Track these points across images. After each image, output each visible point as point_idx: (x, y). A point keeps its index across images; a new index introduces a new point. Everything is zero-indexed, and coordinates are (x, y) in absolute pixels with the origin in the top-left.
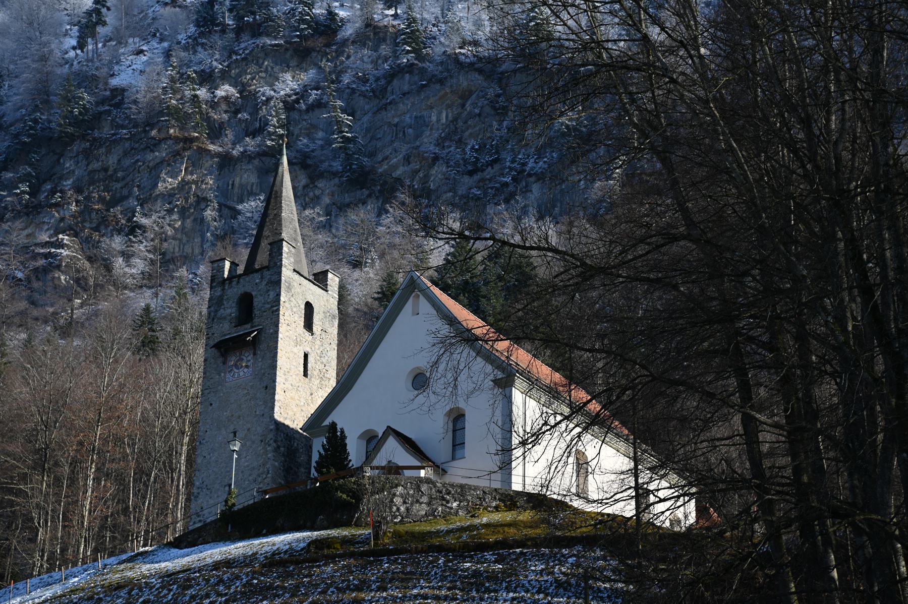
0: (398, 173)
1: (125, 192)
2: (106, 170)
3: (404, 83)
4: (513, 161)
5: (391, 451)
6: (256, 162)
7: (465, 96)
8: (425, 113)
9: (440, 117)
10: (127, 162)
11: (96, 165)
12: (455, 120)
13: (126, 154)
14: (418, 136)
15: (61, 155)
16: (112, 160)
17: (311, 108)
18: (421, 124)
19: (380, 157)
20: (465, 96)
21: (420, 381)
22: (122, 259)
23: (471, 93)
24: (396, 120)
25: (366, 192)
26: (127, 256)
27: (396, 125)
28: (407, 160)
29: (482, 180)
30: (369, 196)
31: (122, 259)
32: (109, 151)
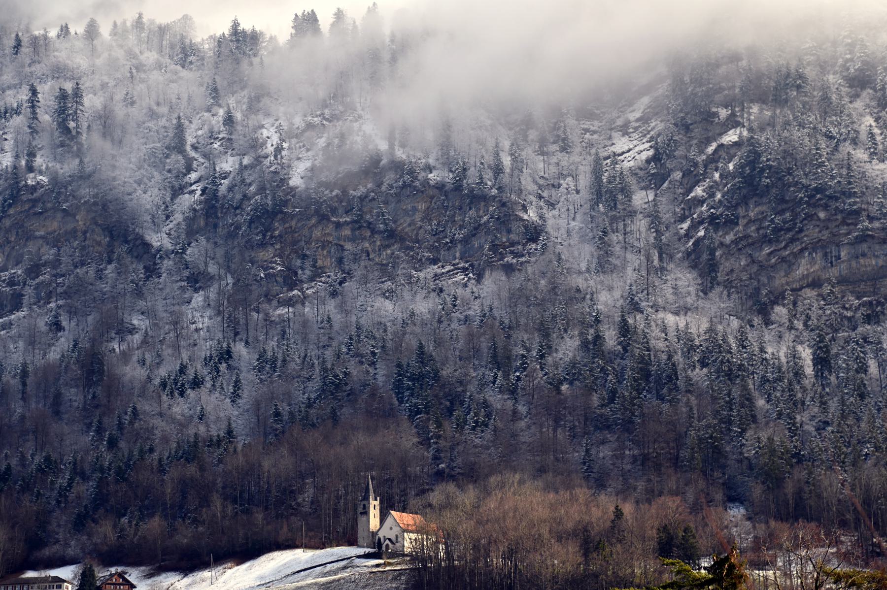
0: (406, 230)
1: (299, 238)
2: (291, 227)
3: (408, 191)
4: (450, 232)
5: (387, 542)
6: (350, 225)
7: (432, 197)
8: (416, 205)
9: (422, 206)
10: (299, 225)
11: (287, 225)
12: (428, 208)
13: (299, 221)
14: (413, 215)
15: (273, 220)
16: (293, 223)
17: (371, 201)
18: (415, 209)
19: (399, 223)
20: (432, 197)
21: (391, 528)
22: (292, 183)
23: (434, 197)
24: (405, 207)
25: (394, 240)
26: (303, 269)
27: (404, 210)
28: (410, 225)
29: (439, 238)
30: (395, 242)
31: (292, 183)
32: (292, 219)
